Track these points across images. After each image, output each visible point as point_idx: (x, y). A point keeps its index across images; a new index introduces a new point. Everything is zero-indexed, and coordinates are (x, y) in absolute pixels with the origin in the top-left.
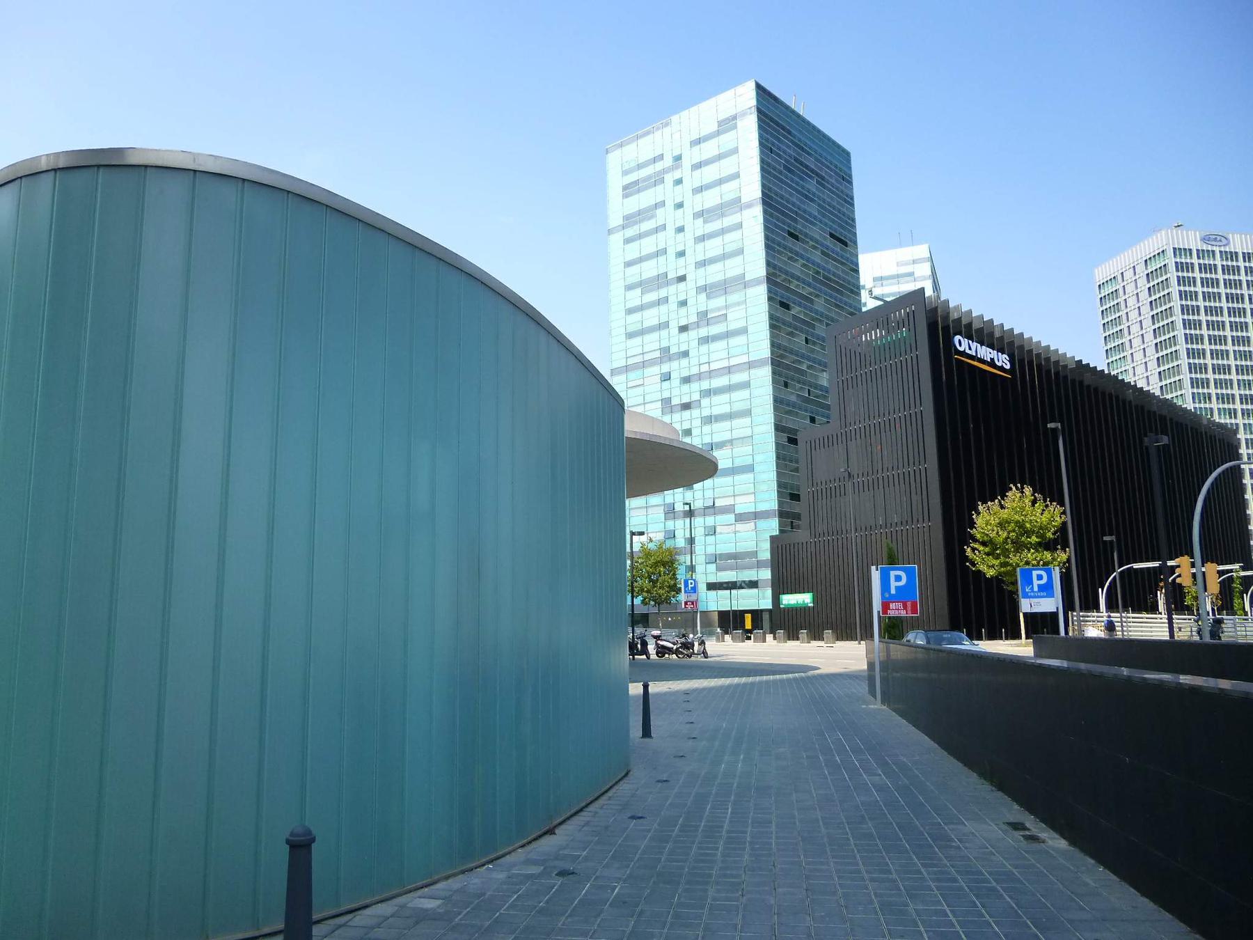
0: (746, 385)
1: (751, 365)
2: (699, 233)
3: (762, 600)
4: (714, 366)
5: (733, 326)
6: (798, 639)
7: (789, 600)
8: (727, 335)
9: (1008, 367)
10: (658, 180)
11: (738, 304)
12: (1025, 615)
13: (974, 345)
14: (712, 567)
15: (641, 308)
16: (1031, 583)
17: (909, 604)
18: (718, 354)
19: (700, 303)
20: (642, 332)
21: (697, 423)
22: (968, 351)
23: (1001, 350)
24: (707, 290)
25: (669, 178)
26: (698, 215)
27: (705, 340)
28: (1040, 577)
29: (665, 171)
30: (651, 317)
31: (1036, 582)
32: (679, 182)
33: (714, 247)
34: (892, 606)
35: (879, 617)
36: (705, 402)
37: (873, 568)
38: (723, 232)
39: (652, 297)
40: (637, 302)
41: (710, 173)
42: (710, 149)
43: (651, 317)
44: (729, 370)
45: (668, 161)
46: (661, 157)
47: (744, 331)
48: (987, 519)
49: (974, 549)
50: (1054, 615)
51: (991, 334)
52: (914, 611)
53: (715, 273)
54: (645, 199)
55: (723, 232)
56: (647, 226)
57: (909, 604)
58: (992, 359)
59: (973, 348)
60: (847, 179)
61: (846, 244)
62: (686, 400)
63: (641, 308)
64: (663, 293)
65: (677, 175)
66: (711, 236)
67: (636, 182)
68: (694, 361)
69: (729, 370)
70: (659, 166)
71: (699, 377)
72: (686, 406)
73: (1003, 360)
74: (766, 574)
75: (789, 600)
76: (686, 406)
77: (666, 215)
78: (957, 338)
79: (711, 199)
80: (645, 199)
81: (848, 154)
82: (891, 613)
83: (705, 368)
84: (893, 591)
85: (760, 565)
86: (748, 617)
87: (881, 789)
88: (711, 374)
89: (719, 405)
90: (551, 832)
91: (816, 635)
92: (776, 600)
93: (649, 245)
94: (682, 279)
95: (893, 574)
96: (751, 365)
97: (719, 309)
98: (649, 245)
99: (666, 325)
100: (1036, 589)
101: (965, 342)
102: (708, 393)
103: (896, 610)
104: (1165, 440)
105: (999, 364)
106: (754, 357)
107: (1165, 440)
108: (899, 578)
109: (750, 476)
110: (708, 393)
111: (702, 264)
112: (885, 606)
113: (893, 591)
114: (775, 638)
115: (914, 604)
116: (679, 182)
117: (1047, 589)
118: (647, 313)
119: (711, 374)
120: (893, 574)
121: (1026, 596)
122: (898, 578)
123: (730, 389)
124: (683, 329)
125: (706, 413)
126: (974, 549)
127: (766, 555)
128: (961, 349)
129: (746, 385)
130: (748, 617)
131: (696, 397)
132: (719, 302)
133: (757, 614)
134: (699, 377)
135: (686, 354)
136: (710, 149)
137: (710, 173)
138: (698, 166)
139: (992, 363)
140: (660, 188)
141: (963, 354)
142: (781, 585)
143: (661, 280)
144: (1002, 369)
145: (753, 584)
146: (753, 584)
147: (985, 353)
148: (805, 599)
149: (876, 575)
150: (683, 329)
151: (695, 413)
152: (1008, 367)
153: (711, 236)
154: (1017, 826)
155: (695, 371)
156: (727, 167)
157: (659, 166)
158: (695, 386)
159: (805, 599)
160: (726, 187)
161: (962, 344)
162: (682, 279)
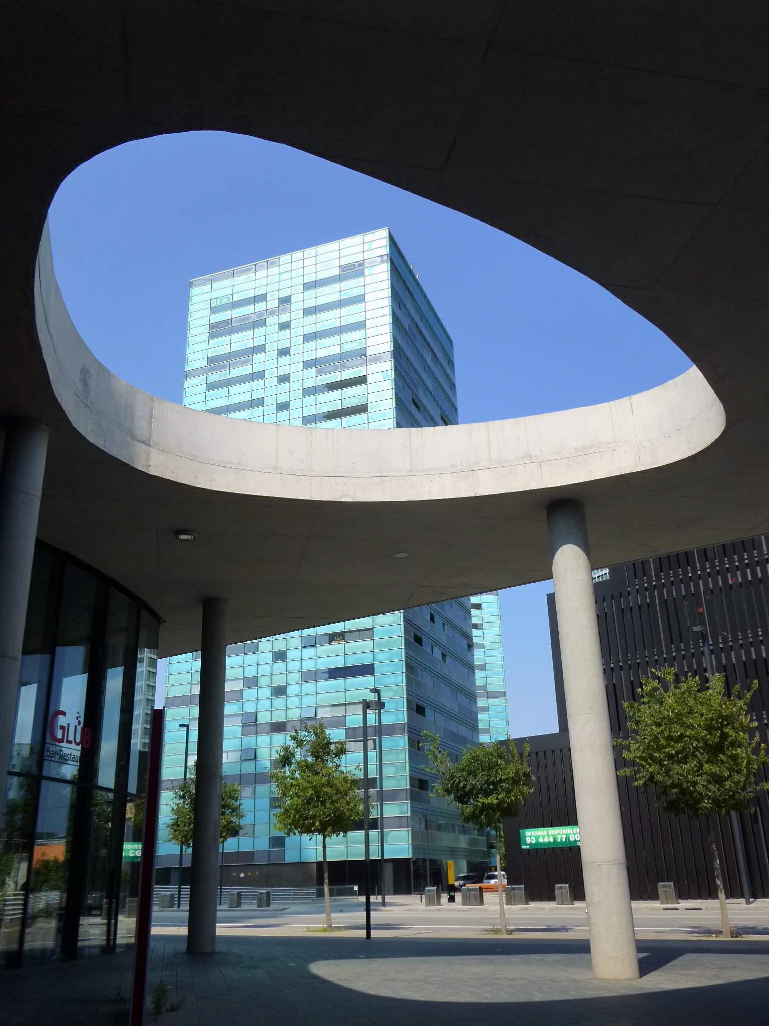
2: (310, 384)
25: (272, 321)
41: (328, 320)
42: (328, 294)
46: (263, 298)
68: (293, 702)
136: (328, 294)
137: (328, 320)
156: (350, 314)
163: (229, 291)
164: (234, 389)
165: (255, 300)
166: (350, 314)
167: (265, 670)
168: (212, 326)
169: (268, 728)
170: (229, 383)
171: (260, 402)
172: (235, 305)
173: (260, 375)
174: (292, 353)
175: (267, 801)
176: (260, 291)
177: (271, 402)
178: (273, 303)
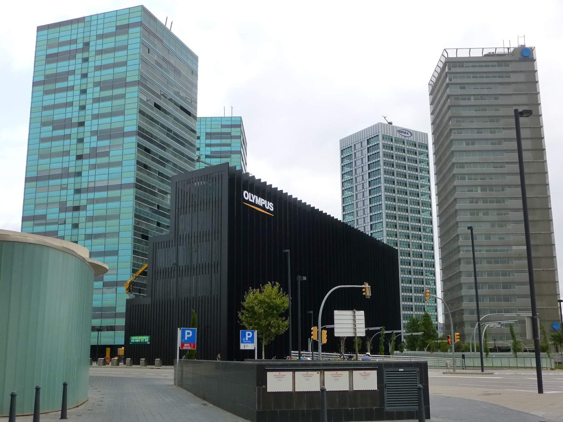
0: (118, 199)
1: (121, 187)
2: (96, 95)
3: (119, 338)
4: (98, 184)
5: (112, 160)
6: (139, 364)
7: (135, 339)
8: (109, 165)
9: (272, 210)
10: (71, 55)
11: (118, 145)
12: (423, 368)
13: (254, 197)
14: (95, 138)
15: (52, 139)
16: (245, 336)
17: (192, 345)
18: (101, 177)
19: (91, 142)
20: (51, 155)
21: (83, 219)
22: (250, 200)
23: (269, 200)
24: (101, 135)
25: (79, 56)
26: (96, 84)
27: (94, 167)
28: (249, 335)
29: (77, 51)
30: (57, 146)
31: (247, 337)
33: (106, 106)
34: (185, 345)
35: (180, 350)
36: (90, 207)
37: (179, 329)
39: (61, 132)
40: (49, 135)
41: (108, 59)
42: (109, 43)
43: (57, 146)
44: (108, 188)
46: (75, 41)
47: (120, 164)
48: (252, 298)
49: (243, 314)
50: (253, 351)
51: (264, 191)
52: (194, 347)
53: (105, 124)
54: (63, 66)
55: (112, 98)
56: (59, 85)
57: (192, 345)
58: (264, 205)
59: (254, 199)
60: (194, 73)
62: (76, 204)
63: (52, 139)
64: (67, 131)
65: (85, 55)
67: (57, 54)
68: (84, 179)
69: (108, 188)
71: (88, 190)
72: (76, 209)
73: (270, 206)
74: (121, 322)
75: (135, 339)
77: (74, 81)
78: (245, 192)
79: (107, 75)
80: (63, 66)
81: (195, 58)
82: (185, 348)
83: (91, 185)
84: (186, 339)
85: (116, 316)
86: (108, 350)
88: (95, 189)
89: (99, 209)
90: (78, 406)
91: (150, 362)
92: (127, 339)
93: (61, 98)
94: (82, 124)
95: (186, 331)
96: (121, 187)
97: (104, 147)
98: (61, 98)
99: (67, 153)
100: (247, 339)
101: (249, 195)
102: (93, 201)
103: (187, 347)
104: (305, 278)
105: (268, 208)
106: (124, 181)
107: (305, 278)
108: (189, 333)
109: (115, 258)
110: (93, 201)
111: (96, 117)
112: (182, 345)
113: (186, 339)
114: (125, 364)
115: (194, 344)
117: (251, 340)
118: (55, 143)
119: (95, 189)
120: (186, 331)
121: (242, 342)
122: (189, 334)
123: (107, 200)
124: (79, 157)
125: (90, 214)
126: (243, 314)
127: (122, 309)
128: (247, 199)
129: (118, 199)
130: (108, 350)
131: (83, 203)
132: (106, 143)
133: (114, 348)
134: (88, 190)
136: (109, 43)
137: (108, 59)
138: (100, 52)
139: (263, 207)
141: (248, 201)
142: (130, 331)
143: (66, 124)
144: (268, 211)
145: (112, 328)
146: (112, 328)
147: (261, 201)
148: (145, 339)
149: (179, 332)
150: (79, 157)
151: (82, 213)
152: (272, 210)
154: (205, 405)
155: (84, 185)
156: (120, 56)
158: (84, 196)
159: (145, 339)
160: (117, 70)
161: (248, 196)
162: (82, 124)
163: (57, 35)
164: (58, 95)
165: (70, 42)
166: (120, 56)
167: (79, 66)
168: (48, 56)
169: (77, 124)
170: (55, 91)
171: (71, 104)
172: (61, 44)
173: (72, 88)
174: (87, 92)
175: (78, 108)
176: (74, 37)
177: (73, 153)
178: (80, 46)
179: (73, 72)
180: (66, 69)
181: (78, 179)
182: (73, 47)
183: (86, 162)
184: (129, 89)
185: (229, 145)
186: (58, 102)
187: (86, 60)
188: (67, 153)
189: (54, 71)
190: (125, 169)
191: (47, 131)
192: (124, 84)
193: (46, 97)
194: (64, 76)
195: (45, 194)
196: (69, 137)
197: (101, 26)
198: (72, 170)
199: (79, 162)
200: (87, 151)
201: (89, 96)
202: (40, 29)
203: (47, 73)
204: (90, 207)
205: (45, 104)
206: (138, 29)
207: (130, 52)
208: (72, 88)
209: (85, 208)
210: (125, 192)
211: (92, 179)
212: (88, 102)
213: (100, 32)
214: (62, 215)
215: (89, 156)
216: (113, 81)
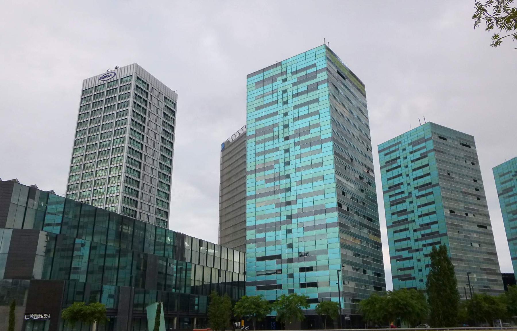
2: (411, 150)
14: (411, 146)
21: (415, 211)
26: (416, 188)
29: (406, 198)
32: (411, 202)
36: (299, 201)
38: (427, 194)
41: (304, 111)
45: (406, 194)
61: (469, 147)
62: (288, 200)
64: (407, 226)
65: (411, 199)
66: (415, 151)
68: (403, 144)
70: (403, 195)
72: (418, 250)
76: (418, 250)
77: (279, 130)
87: (504, 21)
98: (269, 146)
99: (277, 149)
116: (411, 202)
124: (287, 138)
131: (421, 247)
135: (413, 212)
140: (404, 204)
150: (287, 138)
151: (294, 207)
153: (415, 151)
157: (403, 195)
166: (313, 108)
167: (281, 108)
170: (265, 141)
173: (277, 137)
178: (284, 218)
179: (277, 125)
180: (271, 123)
181: (288, 194)
182: (278, 219)
183: (292, 141)
184: (324, 145)
185: (425, 147)
186: (267, 148)
187: (285, 80)
188: (277, 149)
189: (262, 126)
190: (327, 196)
191: (396, 218)
192: (320, 141)
193: (258, 146)
194: (270, 129)
195: (263, 208)
196: (398, 149)
197: (295, 65)
198: (282, 174)
199: (287, 142)
200: (292, 133)
201: (292, 153)
202: (249, 76)
203: (257, 128)
204: (299, 201)
205: (257, 117)
206: (326, 85)
207: (325, 168)
208: (277, 137)
209: (295, 202)
210: (330, 230)
211: (297, 127)
212: (289, 109)
213: (294, 70)
214: (278, 210)
215: (294, 136)
216: (418, 140)
